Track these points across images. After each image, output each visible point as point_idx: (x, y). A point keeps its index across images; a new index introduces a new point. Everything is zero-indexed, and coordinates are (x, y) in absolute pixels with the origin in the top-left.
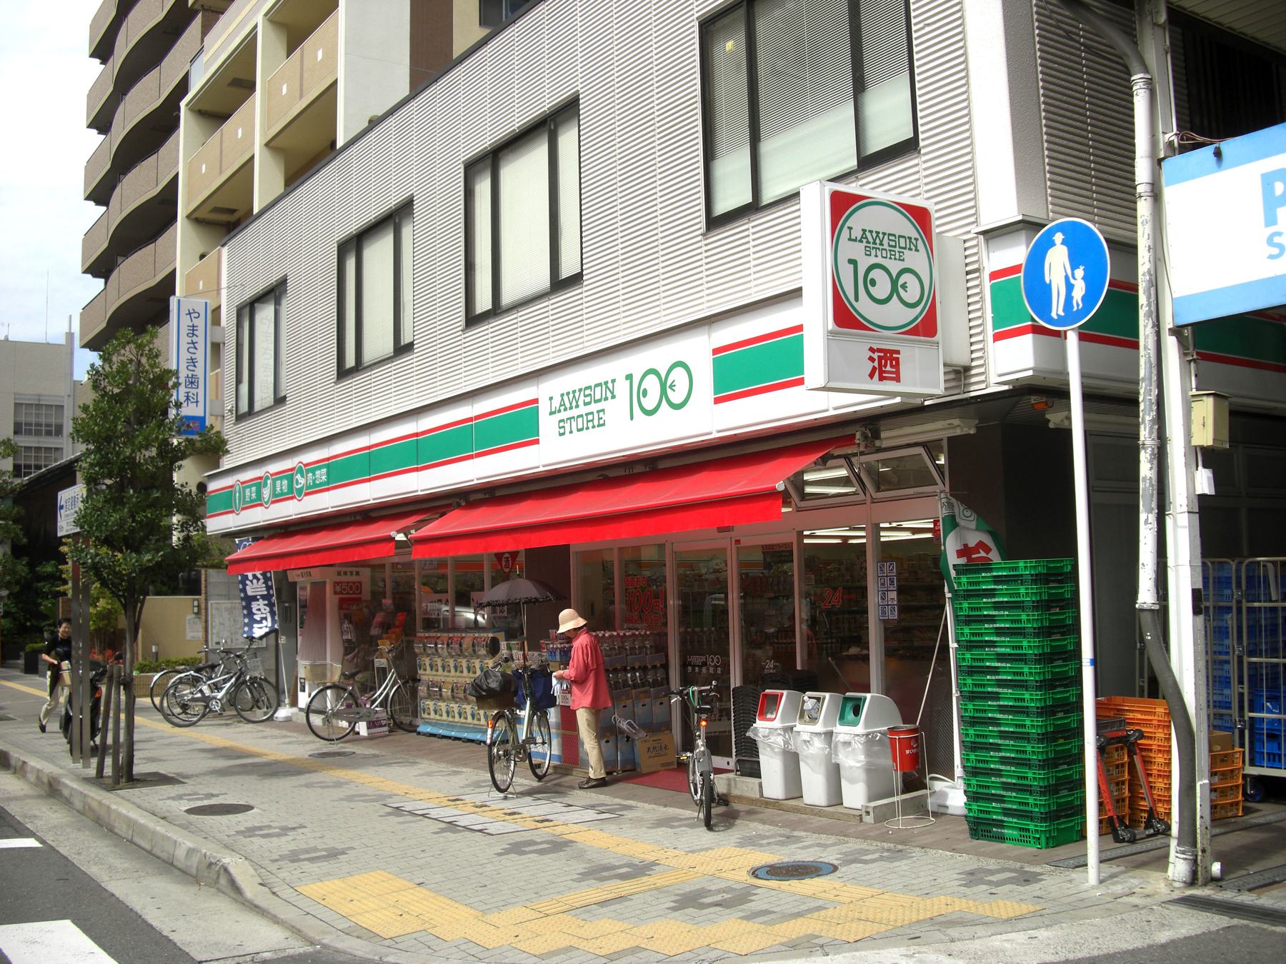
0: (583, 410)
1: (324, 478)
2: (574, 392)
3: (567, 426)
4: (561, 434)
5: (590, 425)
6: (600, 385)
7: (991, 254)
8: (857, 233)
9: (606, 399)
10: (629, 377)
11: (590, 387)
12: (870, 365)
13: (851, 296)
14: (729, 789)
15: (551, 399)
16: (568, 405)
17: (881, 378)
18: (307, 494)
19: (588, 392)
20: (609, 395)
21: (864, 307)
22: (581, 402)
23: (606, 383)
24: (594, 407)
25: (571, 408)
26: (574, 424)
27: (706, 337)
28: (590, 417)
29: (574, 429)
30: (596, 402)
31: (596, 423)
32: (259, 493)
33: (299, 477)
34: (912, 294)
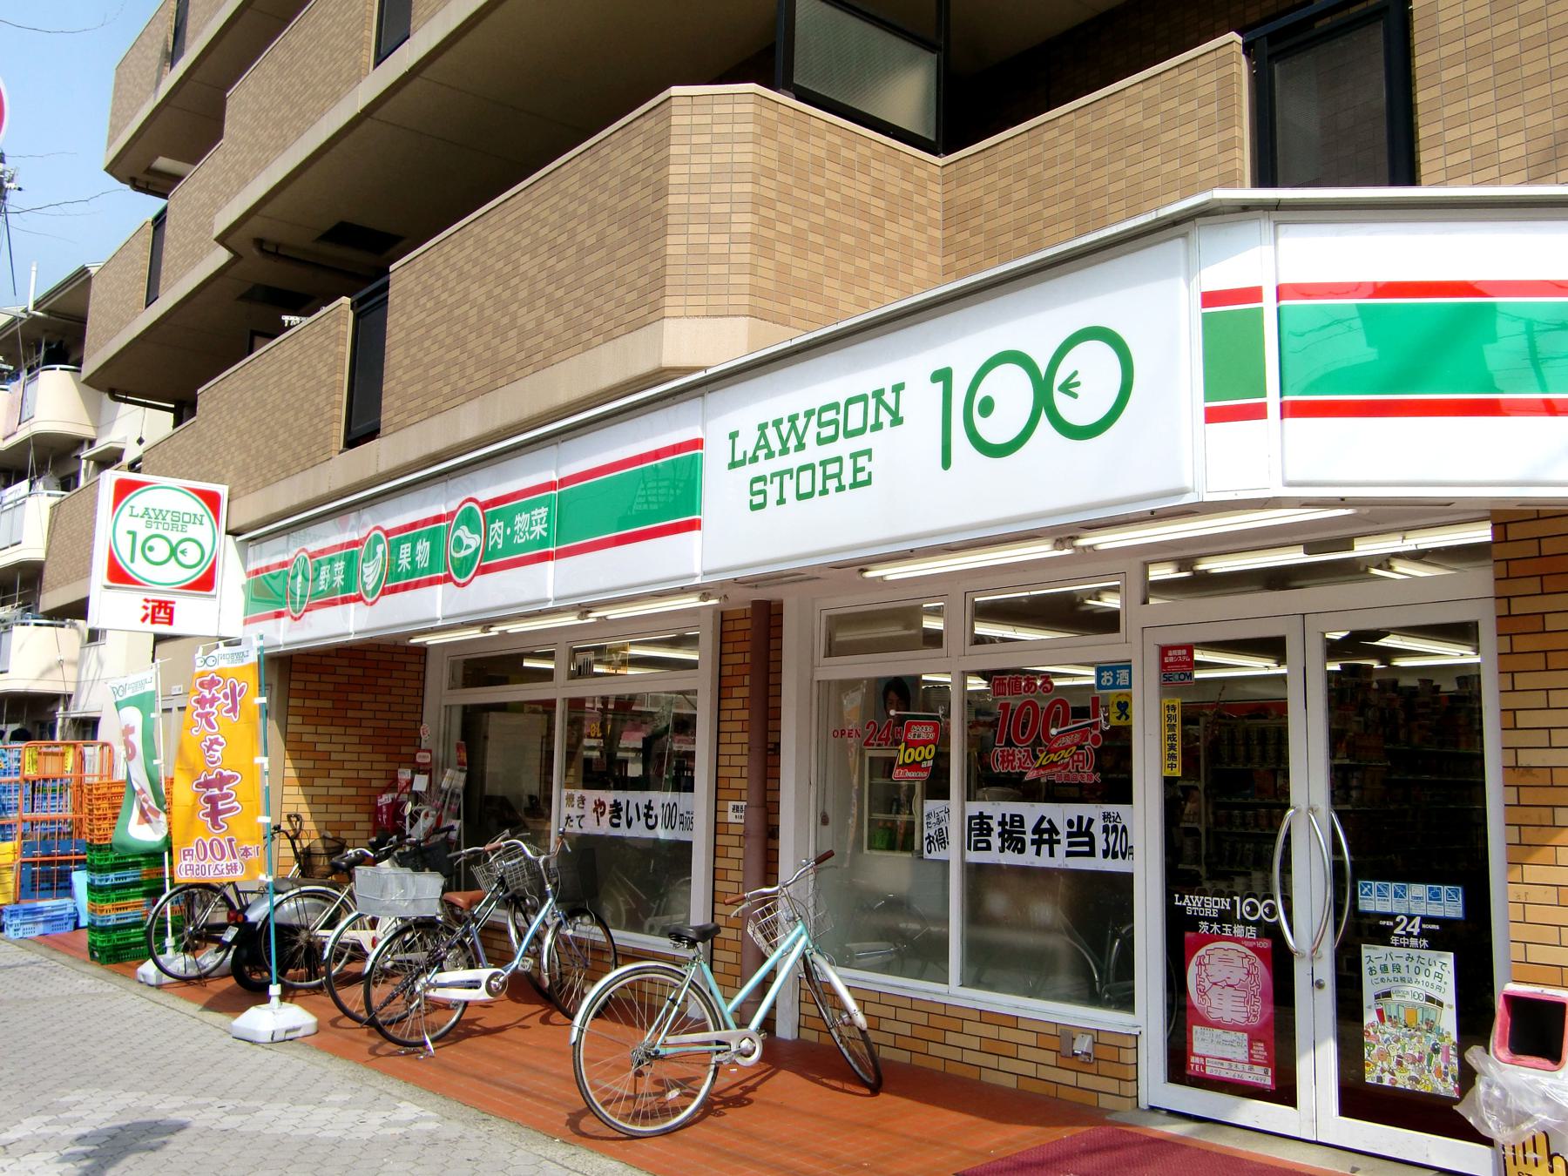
0: (813, 453)
1: (539, 529)
2: (793, 419)
3: (773, 491)
4: (754, 507)
5: (832, 484)
6: (863, 398)
7: (1281, 241)
8: (139, 510)
9: (877, 426)
10: (943, 376)
11: (834, 406)
12: (144, 612)
13: (127, 558)
14: (227, 975)
15: (733, 436)
16: (776, 445)
17: (153, 622)
18: (484, 570)
19: (829, 416)
20: (885, 417)
21: (138, 568)
22: (810, 439)
23: (878, 394)
24: (843, 447)
25: (784, 451)
26: (790, 485)
27: (1268, 249)
28: (833, 469)
29: (790, 492)
30: (849, 434)
31: (847, 479)
32: (351, 572)
33: (463, 532)
34: (193, 555)
